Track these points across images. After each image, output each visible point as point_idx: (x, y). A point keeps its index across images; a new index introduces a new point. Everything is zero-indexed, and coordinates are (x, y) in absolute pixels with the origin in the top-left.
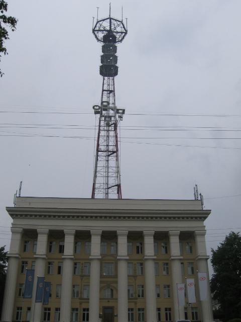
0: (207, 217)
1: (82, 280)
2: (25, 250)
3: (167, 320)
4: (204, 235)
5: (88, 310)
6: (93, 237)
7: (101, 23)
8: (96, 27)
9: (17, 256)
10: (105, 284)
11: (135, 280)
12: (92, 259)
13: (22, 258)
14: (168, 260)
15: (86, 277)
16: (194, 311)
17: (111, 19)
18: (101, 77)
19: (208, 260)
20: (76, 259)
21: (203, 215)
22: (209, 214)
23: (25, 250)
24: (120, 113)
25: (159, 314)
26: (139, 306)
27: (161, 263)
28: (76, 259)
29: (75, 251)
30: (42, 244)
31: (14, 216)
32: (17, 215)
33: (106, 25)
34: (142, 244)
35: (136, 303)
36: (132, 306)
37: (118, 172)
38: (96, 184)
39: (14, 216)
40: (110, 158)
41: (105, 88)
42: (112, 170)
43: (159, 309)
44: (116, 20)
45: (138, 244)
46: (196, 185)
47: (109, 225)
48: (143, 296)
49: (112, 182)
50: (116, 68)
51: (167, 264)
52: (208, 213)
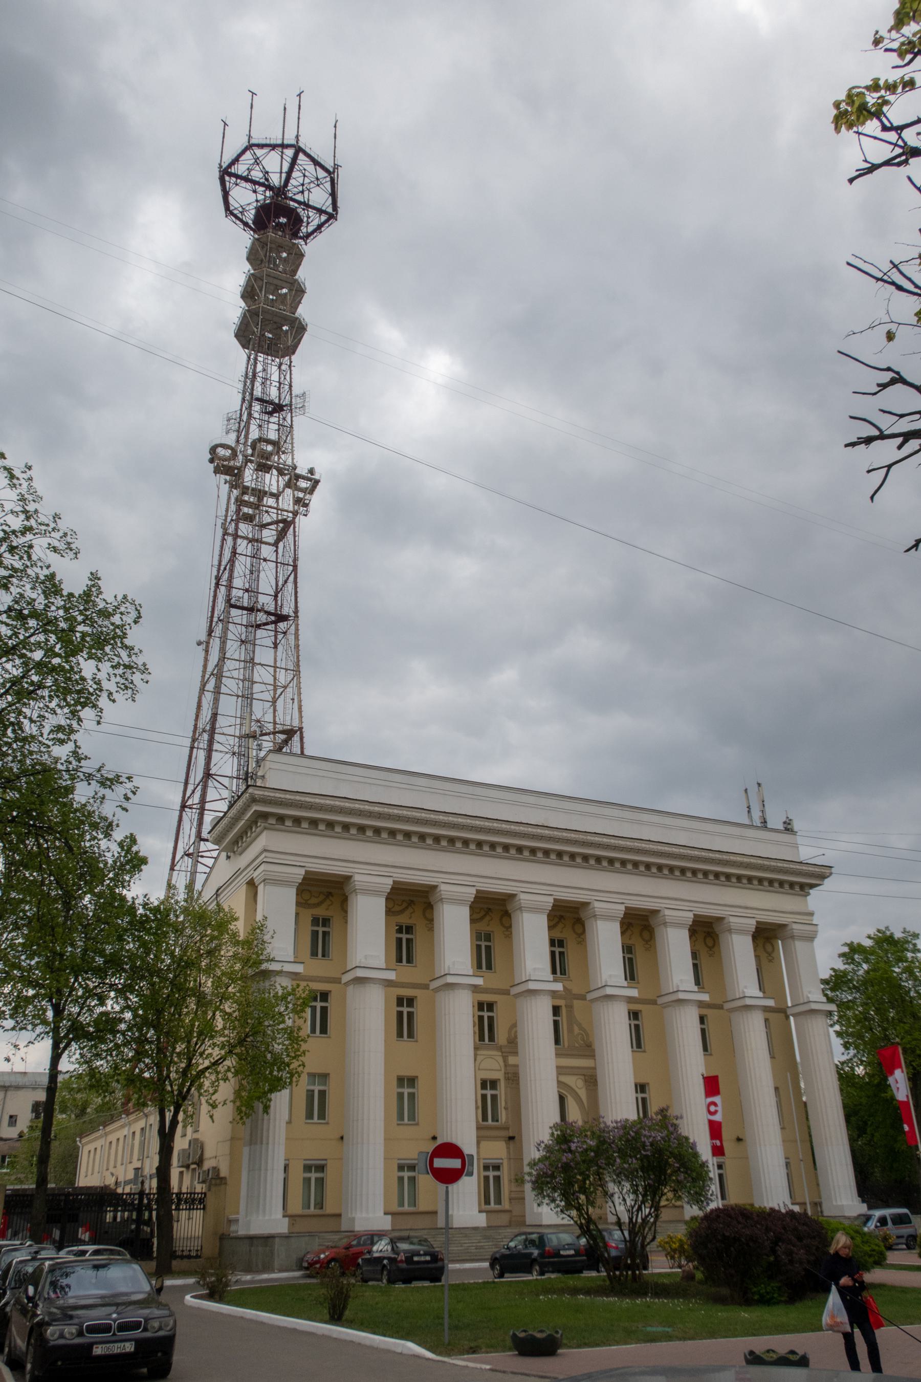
3: (310, 1115)
4: (811, 938)
7: (259, 152)
8: (236, 161)
15: (585, 1047)
16: (317, 1088)
17: (299, 150)
18: (239, 355)
21: (803, 880)
22: (823, 877)
24: (301, 490)
33: (274, 163)
40: (260, 633)
41: (258, 392)
44: (316, 163)
47: (573, 883)
50: (300, 329)
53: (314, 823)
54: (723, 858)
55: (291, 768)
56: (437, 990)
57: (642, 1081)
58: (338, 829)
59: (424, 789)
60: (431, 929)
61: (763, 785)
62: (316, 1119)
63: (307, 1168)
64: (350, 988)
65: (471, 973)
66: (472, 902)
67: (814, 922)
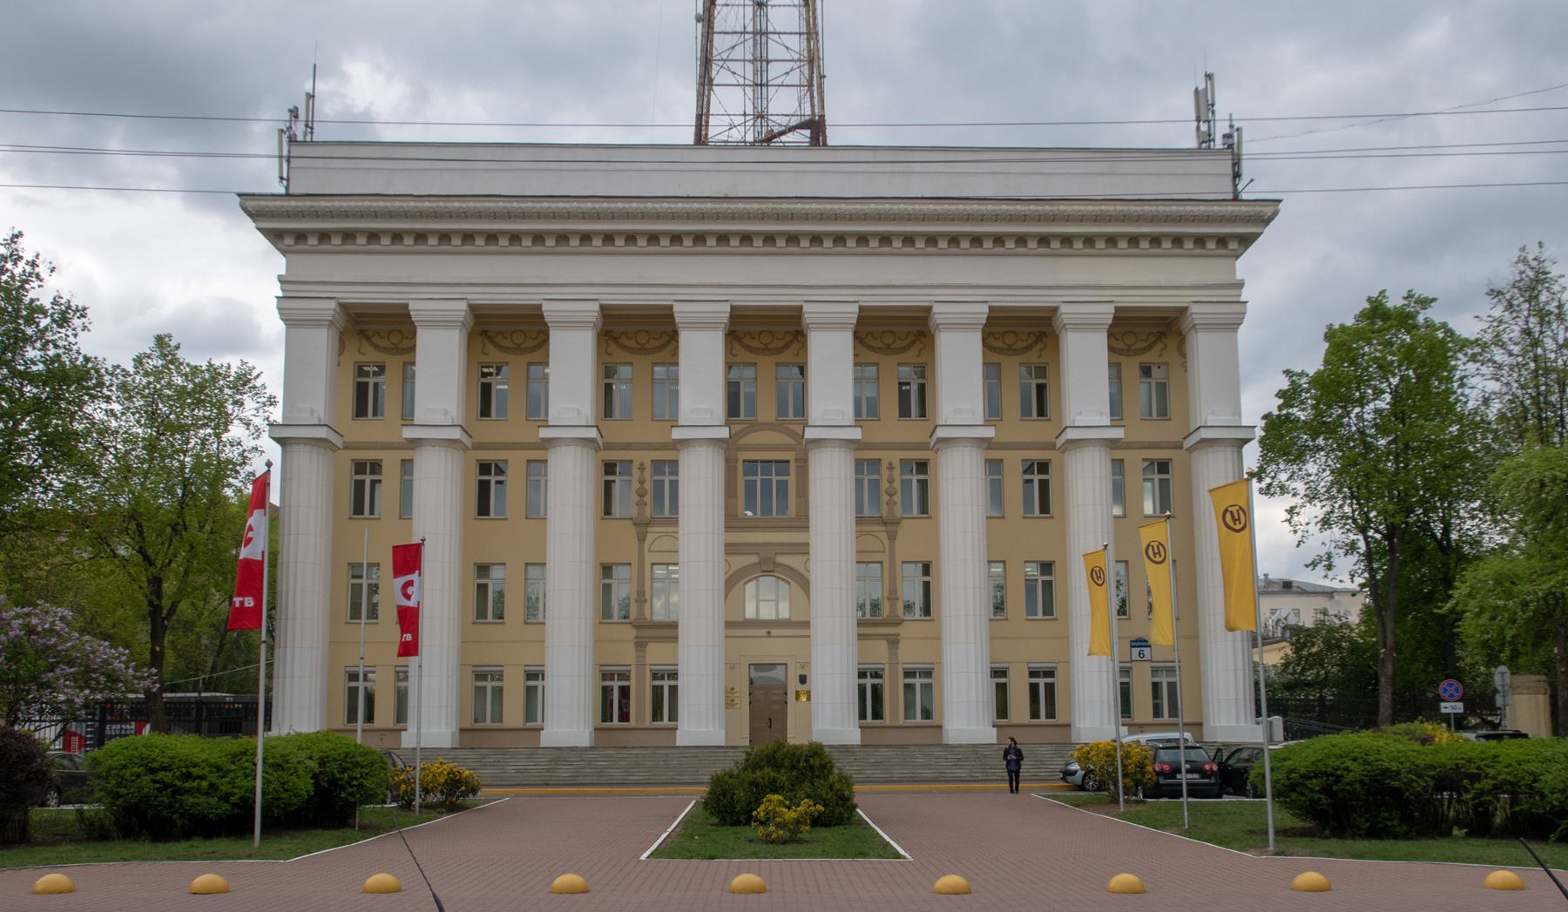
0: (1256, 236)
1: (642, 539)
2: (485, 411)
4: (1233, 325)
5: (674, 675)
6: (685, 337)
9: (322, 433)
10: (753, 559)
11: (892, 538)
12: (685, 443)
13: (478, 446)
14: (924, 446)
19: (1247, 449)
20: (609, 447)
21: (1233, 228)
22: (1267, 221)
23: (485, 411)
25: (1001, 690)
26: (911, 654)
27: (1135, 461)
28: (609, 447)
29: (607, 396)
30: (439, 376)
31: (289, 241)
32: (301, 236)
34: (925, 370)
35: (893, 642)
36: (878, 654)
37: (812, 60)
38: (712, 120)
39: (289, 241)
42: (785, 48)
43: (998, 673)
45: (906, 372)
46: (1209, 77)
48: (927, 610)
49: (785, 104)
51: (1043, 467)
52: (1263, 215)
53: (349, 236)
54: (726, 207)
55: (320, 163)
56: (1192, 449)
57: (608, 560)
58: (965, 244)
59: (526, 166)
60: (1184, 366)
61: (1216, 78)
62: (1040, 615)
63: (1033, 674)
64: (1196, 455)
65: (981, 422)
66: (986, 326)
67: (1243, 299)
